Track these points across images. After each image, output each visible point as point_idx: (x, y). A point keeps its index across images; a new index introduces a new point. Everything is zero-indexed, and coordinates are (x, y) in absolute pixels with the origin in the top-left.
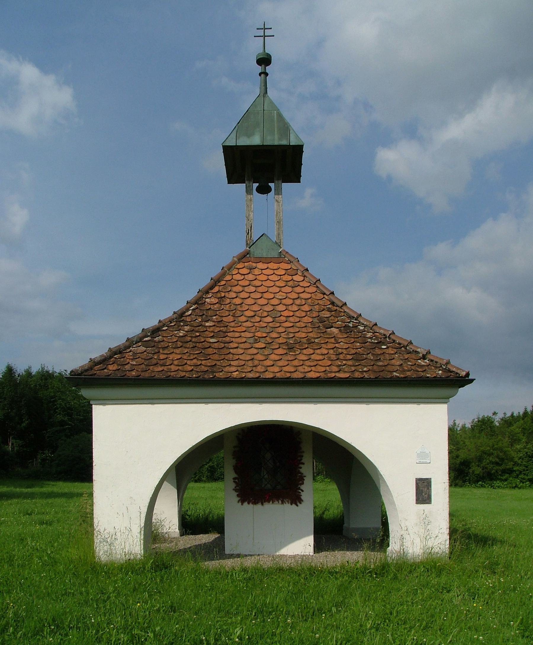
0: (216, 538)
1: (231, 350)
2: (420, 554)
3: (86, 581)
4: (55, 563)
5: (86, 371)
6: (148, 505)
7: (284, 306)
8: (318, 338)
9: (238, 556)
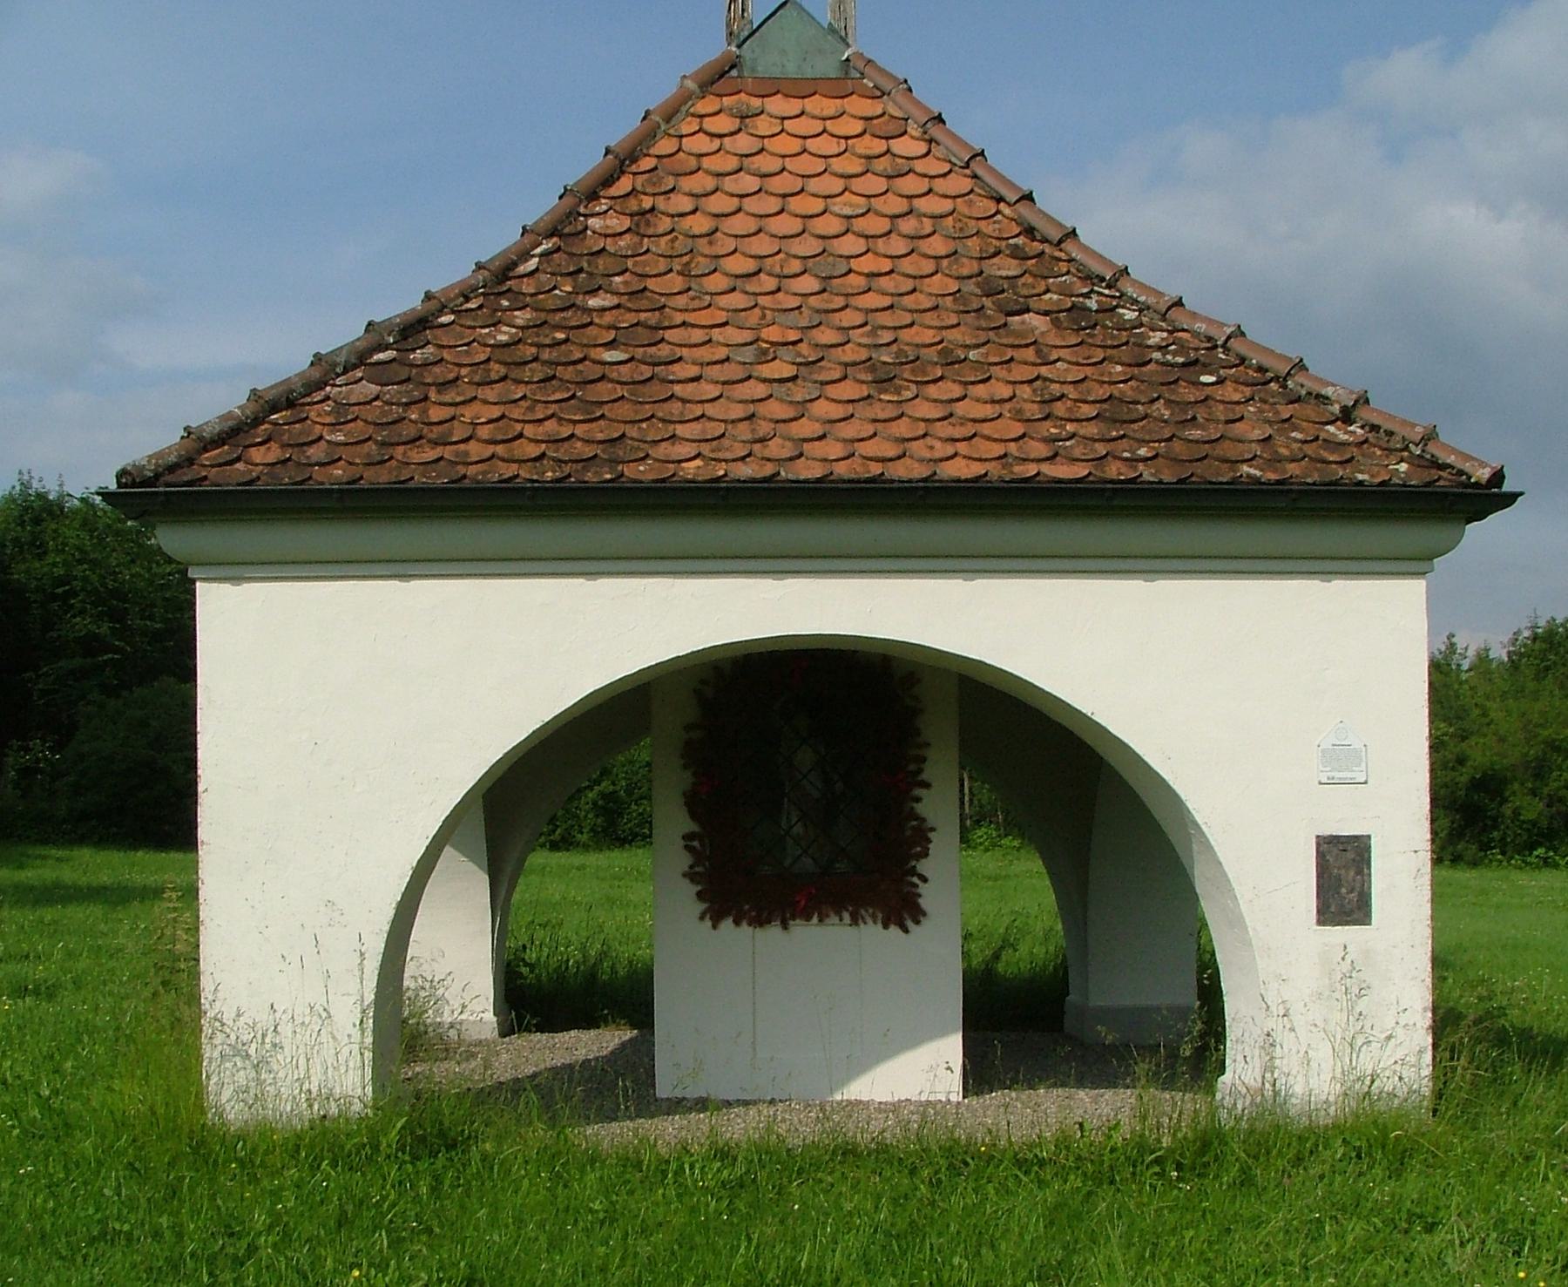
0: (623, 1045)
1: (677, 389)
2: (1332, 1099)
3: (174, 1192)
4: (67, 1127)
5: (172, 468)
6: (387, 928)
7: (862, 241)
8: (977, 346)
9: (702, 1104)
